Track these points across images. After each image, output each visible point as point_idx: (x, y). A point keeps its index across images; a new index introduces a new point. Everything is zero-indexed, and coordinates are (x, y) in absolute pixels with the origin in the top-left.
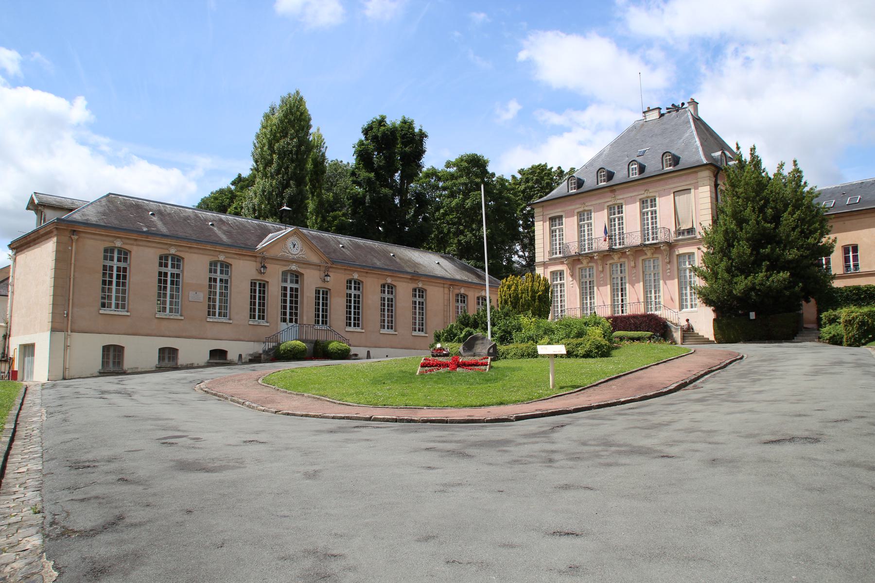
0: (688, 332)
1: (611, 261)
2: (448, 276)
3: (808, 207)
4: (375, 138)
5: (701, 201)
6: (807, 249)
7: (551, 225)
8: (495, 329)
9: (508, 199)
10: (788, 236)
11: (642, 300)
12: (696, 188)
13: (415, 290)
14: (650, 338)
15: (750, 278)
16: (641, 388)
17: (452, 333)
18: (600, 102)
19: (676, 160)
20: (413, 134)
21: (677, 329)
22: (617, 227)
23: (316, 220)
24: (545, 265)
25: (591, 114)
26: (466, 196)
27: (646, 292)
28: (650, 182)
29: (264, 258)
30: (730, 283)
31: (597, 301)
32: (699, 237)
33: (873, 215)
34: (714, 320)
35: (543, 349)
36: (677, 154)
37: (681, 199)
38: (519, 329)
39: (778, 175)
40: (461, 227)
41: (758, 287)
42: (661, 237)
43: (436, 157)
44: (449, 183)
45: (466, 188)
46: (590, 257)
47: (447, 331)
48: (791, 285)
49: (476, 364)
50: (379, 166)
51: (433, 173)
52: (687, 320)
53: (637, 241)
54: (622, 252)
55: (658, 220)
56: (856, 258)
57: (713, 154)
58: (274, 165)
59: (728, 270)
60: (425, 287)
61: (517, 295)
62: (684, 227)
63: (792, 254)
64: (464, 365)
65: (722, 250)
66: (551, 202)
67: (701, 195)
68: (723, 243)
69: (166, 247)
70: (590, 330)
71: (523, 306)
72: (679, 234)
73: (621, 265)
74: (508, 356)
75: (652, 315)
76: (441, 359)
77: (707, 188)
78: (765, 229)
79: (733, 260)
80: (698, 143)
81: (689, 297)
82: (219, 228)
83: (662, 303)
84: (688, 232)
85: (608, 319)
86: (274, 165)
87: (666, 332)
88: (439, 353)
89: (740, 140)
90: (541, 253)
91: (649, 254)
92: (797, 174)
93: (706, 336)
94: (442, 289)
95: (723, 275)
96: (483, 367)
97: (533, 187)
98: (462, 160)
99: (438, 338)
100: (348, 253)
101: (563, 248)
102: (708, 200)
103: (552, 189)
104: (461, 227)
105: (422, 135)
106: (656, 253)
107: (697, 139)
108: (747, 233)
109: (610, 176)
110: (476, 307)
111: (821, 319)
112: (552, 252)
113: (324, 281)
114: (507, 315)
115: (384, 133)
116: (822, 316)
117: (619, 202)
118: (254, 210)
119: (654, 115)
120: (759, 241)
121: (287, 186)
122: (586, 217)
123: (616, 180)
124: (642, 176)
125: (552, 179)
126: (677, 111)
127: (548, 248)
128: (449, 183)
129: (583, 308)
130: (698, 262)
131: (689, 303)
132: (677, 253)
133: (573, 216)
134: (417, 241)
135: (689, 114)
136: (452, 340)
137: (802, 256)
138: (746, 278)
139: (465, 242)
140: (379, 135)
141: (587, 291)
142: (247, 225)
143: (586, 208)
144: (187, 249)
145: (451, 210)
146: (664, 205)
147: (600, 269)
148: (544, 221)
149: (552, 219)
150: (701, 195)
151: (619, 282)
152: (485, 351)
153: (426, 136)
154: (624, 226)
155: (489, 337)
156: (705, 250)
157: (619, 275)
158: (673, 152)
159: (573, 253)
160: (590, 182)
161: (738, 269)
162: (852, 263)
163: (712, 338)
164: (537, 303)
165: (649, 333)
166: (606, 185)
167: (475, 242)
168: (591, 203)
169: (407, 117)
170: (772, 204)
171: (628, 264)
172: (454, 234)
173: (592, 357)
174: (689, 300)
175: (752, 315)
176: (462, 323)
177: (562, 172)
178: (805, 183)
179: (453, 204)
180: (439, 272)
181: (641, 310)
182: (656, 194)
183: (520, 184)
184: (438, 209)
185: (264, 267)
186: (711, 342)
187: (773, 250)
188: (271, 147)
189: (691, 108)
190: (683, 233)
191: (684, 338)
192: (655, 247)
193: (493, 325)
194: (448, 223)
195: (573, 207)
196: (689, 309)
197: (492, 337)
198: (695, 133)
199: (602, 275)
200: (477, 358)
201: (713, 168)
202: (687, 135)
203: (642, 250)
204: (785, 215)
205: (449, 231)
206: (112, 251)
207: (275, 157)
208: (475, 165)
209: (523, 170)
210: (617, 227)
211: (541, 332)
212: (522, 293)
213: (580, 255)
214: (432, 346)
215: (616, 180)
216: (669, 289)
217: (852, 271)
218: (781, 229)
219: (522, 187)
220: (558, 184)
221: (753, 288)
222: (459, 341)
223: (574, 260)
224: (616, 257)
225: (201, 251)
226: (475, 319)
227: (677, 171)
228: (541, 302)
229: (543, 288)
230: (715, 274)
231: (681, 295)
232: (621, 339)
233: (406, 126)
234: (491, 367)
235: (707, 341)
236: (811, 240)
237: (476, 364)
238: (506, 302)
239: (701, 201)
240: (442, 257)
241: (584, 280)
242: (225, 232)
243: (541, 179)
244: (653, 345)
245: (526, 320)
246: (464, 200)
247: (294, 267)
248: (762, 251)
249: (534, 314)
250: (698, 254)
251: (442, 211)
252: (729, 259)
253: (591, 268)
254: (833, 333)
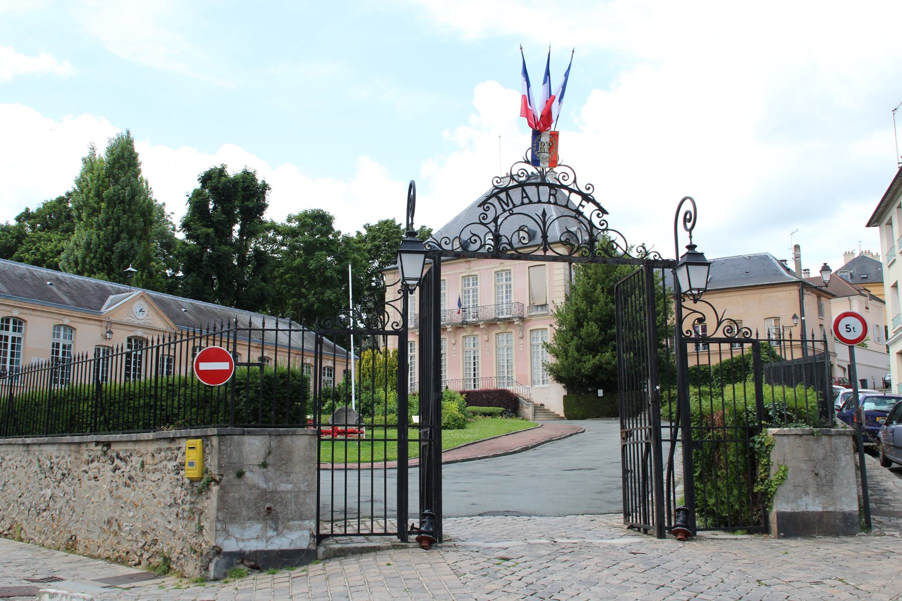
4: (214, 190)
14: (501, 414)
15: (597, 358)
16: (492, 450)
21: (529, 405)
22: (471, 299)
23: (142, 275)
29: (110, 323)
34: (564, 396)
43: (278, 211)
50: (219, 221)
55: (512, 294)
58: (102, 216)
59: (578, 349)
65: (572, 329)
67: (555, 272)
69: (8, 308)
82: (59, 289)
83: (515, 378)
85: (462, 393)
86: (102, 216)
95: (572, 350)
100: (191, 317)
104: (303, 290)
113: (106, 337)
115: (225, 184)
118: (77, 263)
121: (118, 239)
134: (254, 305)
138: (594, 357)
140: (220, 185)
142: (85, 285)
144: (31, 312)
156: (557, 327)
161: (586, 347)
163: (562, 415)
173: (449, 429)
175: (600, 393)
181: (494, 386)
185: (110, 332)
186: (562, 418)
188: (98, 195)
196: (541, 385)
206: (8, 320)
207: (103, 205)
208: (319, 221)
210: (471, 299)
225: (46, 315)
230: (566, 352)
232: (475, 414)
242: (65, 293)
244: (504, 420)
247: (139, 333)
252: (580, 337)
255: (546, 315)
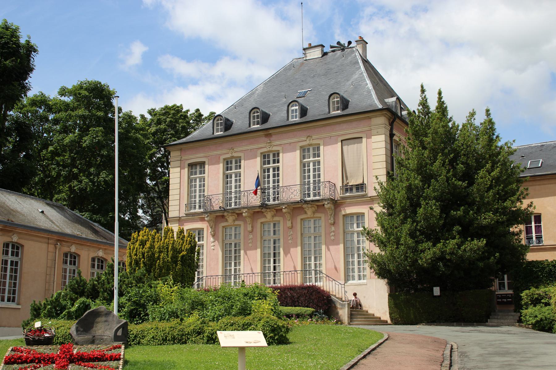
0: (356, 309)
1: (263, 220)
2: (55, 228)
3: (504, 164)
5: (375, 152)
6: (504, 213)
7: (190, 173)
8: (123, 300)
9: (136, 140)
10: (482, 197)
11: (299, 268)
12: (369, 137)
13: (6, 245)
14: (311, 316)
17: (59, 304)
18: (235, 58)
19: (345, 104)
20: (18, 45)
21: (343, 306)
22: (271, 179)
24: (179, 220)
25: (223, 67)
26: (84, 131)
27: (304, 259)
28: (315, 127)
30: (415, 250)
31: (244, 268)
32: (374, 194)
33: (553, 181)
35: (229, 339)
36: (345, 96)
37: (350, 149)
38: (156, 301)
39: (469, 124)
40: (75, 170)
41: (448, 257)
42: (325, 193)
43: (46, 81)
44: (62, 115)
45: (84, 123)
46: (237, 213)
47: (52, 302)
48: (485, 255)
49: (102, 358)
51: (41, 101)
52: (355, 295)
53: (297, 197)
54: (277, 210)
56: (538, 229)
57: (386, 100)
60: (22, 242)
61: (153, 254)
62: (353, 182)
63: (487, 218)
64: (81, 359)
66: (191, 145)
68: (402, 205)
70: (255, 303)
71: (161, 269)
72: (347, 190)
73: (274, 225)
74: (144, 341)
75: (309, 287)
76: (42, 349)
77: (382, 138)
78: (455, 187)
79: (417, 222)
80: (370, 86)
81: (356, 267)
84: (357, 189)
87: (329, 308)
88: (37, 339)
89: (408, 90)
90: (176, 205)
91: (309, 212)
92: (490, 126)
93: (377, 315)
94: (44, 246)
96: (113, 364)
97: (165, 130)
98: (81, 88)
99: (37, 313)
101: (206, 201)
102: (383, 151)
103: (187, 134)
104: (75, 170)
105: (30, 49)
106: (321, 209)
107: (368, 82)
108: (434, 191)
109: (265, 118)
110: (90, 270)
111: (521, 299)
112: (190, 205)
114: (139, 280)
116: (523, 294)
117: (275, 148)
119: (316, 54)
120: (451, 200)
122: (234, 165)
123: (271, 123)
124: (304, 119)
125: (188, 123)
126: (343, 50)
127: (185, 201)
128: (62, 115)
129: (226, 276)
130: (371, 223)
131: (356, 274)
132: (343, 213)
133: (218, 163)
135: (357, 54)
136: (58, 315)
137: (497, 222)
139: (80, 189)
141: (231, 255)
143: (235, 155)
145: (64, 148)
146: (330, 156)
147: (250, 229)
148: (182, 168)
149: (192, 166)
150: (374, 146)
151: (272, 245)
152: (110, 334)
153: (35, 51)
154: (281, 178)
155: (115, 312)
157: (272, 237)
158: (341, 94)
159: (216, 208)
160: (240, 123)
161: (422, 233)
162: (534, 235)
163: (386, 316)
164: (179, 267)
165: (310, 310)
166: (257, 127)
167: (92, 190)
168: (239, 149)
169: (10, 22)
170: (463, 159)
171: (283, 224)
172: (66, 177)
174: (356, 270)
175: (437, 291)
176: (73, 290)
177: (201, 115)
178: (497, 137)
179: (67, 140)
180: (43, 223)
182: (321, 142)
183: (150, 125)
184: (45, 146)
187: (466, 212)
189: (359, 48)
190: (351, 190)
191: (351, 317)
192: (318, 205)
193: (121, 294)
194: (58, 164)
195: (219, 152)
196: (356, 281)
197: (119, 311)
198: (365, 75)
199: (251, 236)
200: (103, 347)
201: (389, 114)
202: (356, 76)
203: (302, 208)
204: (482, 172)
205: (59, 175)
208: (96, 98)
209: (154, 110)
211: (187, 307)
212: (160, 252)
213: (225, 210)
214: (27, 324)
215: (271, 123)
216: (332, 257)
217: (535, 244)
218: (474, 188)
219: (153, 129)
220: (195, 130)
221: (442, 258)
222: (70, 317)
223: (218, 217)
224: (269, 215)
226: (94, 285)
227: (345, 115)
228: (183, 264)
229: (187, 247)
231: (347, 263)
233: (8, 33)
234: (126, 362)
235: (380, 322)
236: (508, 203)
237: (102, 358)
238: (137, 263)
239: (375, 152)
240: (48, 204)
241: (228, 241)
243: (174, 124)
245: (165, 288)
246: (81, 137)
248: (453, 213)
249: (175, 281)
250: (371, 216)
251: (51, 148)
253: (237, 227)
254: (540, 317)
255: (363, 196)
